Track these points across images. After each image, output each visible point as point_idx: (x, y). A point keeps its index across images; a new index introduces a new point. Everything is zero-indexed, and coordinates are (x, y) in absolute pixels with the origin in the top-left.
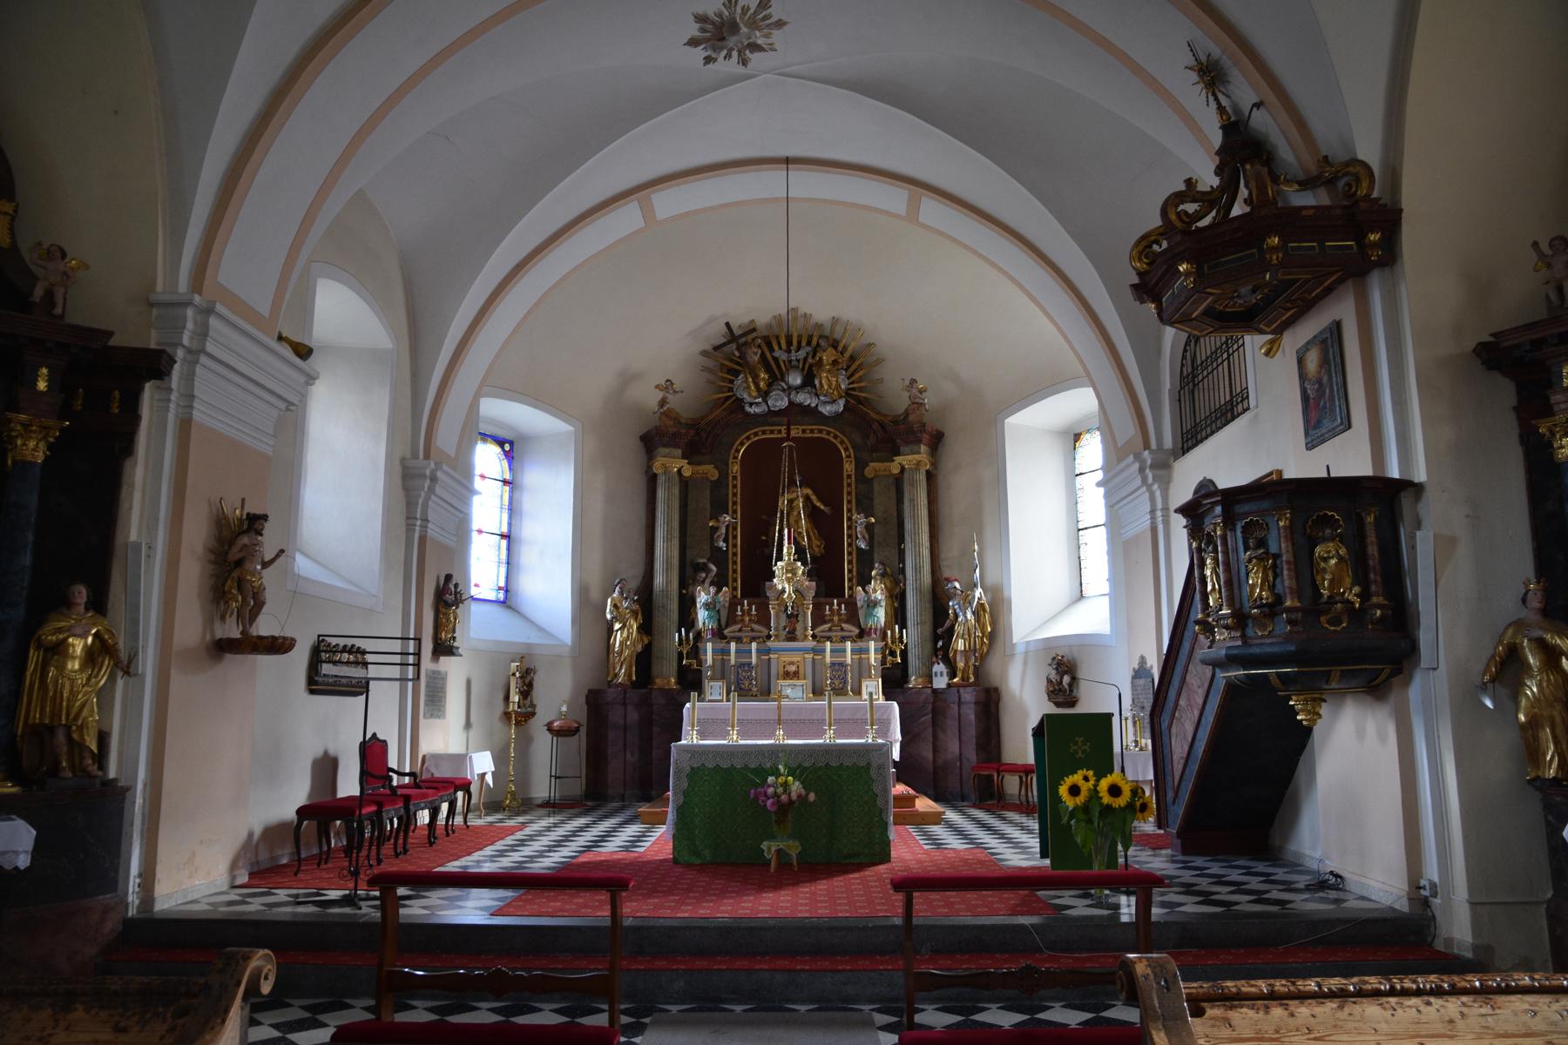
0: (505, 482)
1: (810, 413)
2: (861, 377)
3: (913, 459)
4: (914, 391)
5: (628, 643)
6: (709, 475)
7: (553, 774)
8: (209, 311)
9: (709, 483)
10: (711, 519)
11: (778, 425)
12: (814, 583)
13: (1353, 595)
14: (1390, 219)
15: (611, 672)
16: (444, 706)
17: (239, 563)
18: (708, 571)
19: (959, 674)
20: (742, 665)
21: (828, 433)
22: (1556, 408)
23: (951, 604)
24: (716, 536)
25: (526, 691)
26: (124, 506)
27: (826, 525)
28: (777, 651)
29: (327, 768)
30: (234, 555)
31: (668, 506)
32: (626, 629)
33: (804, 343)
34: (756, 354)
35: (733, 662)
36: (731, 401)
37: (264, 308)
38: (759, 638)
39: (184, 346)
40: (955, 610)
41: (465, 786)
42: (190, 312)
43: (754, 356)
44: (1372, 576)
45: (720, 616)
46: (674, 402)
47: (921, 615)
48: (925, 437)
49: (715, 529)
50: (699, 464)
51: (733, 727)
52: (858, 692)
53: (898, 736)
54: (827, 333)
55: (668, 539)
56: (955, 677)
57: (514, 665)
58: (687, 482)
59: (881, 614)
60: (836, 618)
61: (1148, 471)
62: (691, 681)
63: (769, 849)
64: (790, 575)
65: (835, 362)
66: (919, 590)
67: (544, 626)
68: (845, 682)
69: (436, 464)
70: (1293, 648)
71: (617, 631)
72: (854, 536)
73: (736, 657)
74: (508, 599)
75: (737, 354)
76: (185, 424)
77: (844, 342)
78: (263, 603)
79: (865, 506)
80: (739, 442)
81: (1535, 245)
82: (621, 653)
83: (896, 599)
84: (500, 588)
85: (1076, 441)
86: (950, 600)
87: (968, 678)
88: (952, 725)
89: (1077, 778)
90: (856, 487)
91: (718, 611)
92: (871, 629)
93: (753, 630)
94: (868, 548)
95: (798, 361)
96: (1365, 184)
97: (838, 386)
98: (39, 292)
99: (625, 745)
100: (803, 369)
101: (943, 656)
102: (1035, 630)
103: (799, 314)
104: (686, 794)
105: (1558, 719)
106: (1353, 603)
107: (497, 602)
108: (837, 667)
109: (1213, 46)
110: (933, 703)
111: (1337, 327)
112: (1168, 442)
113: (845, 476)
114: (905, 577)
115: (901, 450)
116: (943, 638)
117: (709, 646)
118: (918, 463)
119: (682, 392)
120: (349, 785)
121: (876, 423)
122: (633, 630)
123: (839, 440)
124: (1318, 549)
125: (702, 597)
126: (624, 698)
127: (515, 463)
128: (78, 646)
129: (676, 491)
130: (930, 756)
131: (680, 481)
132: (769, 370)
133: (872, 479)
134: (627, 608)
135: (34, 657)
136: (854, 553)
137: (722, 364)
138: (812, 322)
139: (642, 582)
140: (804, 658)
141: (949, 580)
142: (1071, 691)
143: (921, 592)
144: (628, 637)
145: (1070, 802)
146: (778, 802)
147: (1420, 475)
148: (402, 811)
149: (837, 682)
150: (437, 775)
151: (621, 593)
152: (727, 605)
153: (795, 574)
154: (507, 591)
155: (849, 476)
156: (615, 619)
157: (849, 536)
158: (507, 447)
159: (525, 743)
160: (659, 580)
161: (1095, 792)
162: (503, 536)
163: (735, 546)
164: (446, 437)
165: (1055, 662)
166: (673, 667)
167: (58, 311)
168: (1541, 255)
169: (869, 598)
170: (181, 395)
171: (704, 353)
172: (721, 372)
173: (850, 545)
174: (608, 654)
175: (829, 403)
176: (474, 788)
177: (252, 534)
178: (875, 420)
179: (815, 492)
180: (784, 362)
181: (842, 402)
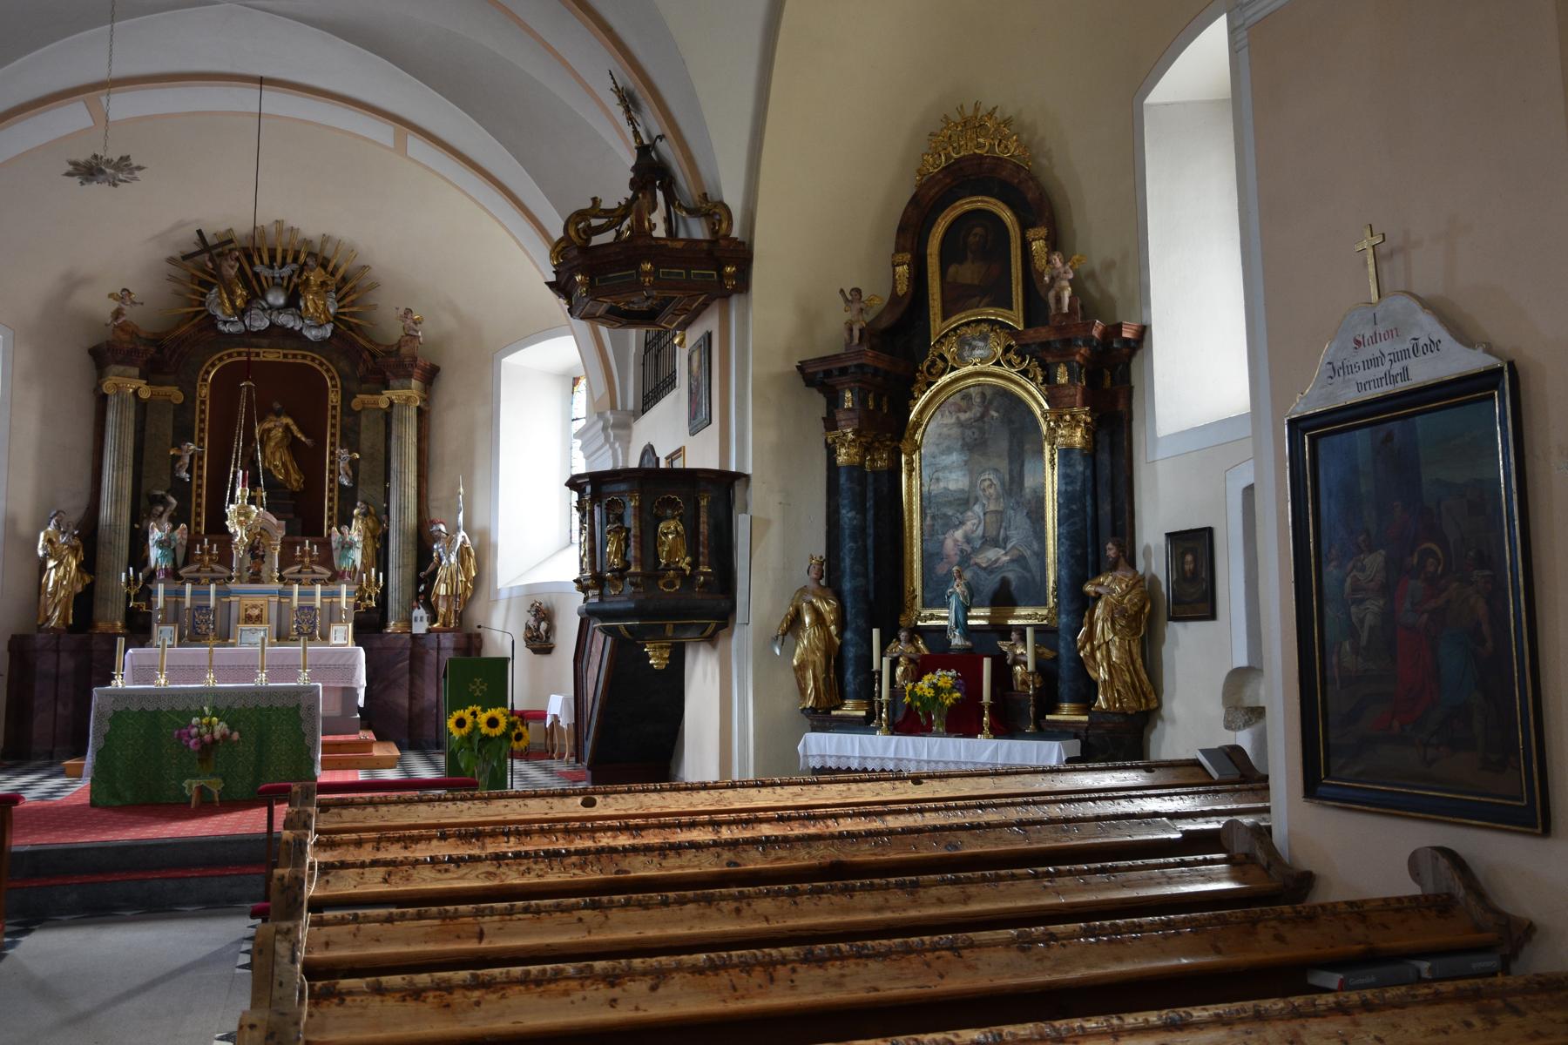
1: (295, 337)
2: (352, 301)
5: (65, 583)
9: (172, 406)
10: (173, 447)
11: (257, 347)
12: (283, 523)
13: (685, 563)
14: (742, 255)
15: (42, 614)
18: (166, 504)
19: (440, 620)
20: (200, 608)
21: (313, 359)
22: (839, 424)
23: (435, 547)
24: (177, 466)
28: (238, 593)
31: (120, 432)
32: (62, 568)
33: (289, 259)
34: (232, 267)
35: (188, 604)
38: (219, 579)
43: (230, 271)
44: (701, 549)
46: (131, 314)
47: (403, 557)
48: (417, 372)
49: (177, 458)
50: (162, 384)
51: (161, 671)
52: (325, 637)
53: (363, 682)
54: (317, 250)
55: (119, 467)
56: (436, 622)
59: (357, 556)
60: (307, 560)
61: (609, 430)
62: (139, 630)
63: (190, 786)
64: (242, 519)
65: (323, 284)
66: (402, 532)
68: (314, 627)
70: (633, 605)
71: (51, 569)
75: (210, 265)
77: (335, 261)
79: (350, 439)
80: (210, 362)
81: (842, 291)
82: (54, 593)
85: (574, 385)
86: (435, 542)
87: (450, 623)
89: (465, 714)
90: (341, 420)
92: (344, 572)
93: (213, 571)
95: (282, 278)
96: (724, 225)
97: (326, 310)
101: (424, 600)
105: (818, 663)
106: (685, 570)
108: (306, 611)
109: (629, 81)
110: (411, 649)
111: (709, 335)
112: (631, 405)
113: (330, 407)
115: (391, 382)
116: (426, 583)
117: (161, 587)
119: (142, 304)
122: (71, 568)
124: (661, 525)
125: (156, 535)
126: (58, 643)
129: (131, 414)
130: (406, 704)
132: (247, 285)
133: (360, 412)
134: (64, 543)
137: (193, 274)
138: (300, 237)
139: (85, 513)
141: (433, 523)
142: (548, 638)
144: (65, 575)
145: (457, 733)
146: (202, 742)
147: (749, 471)
151: (58, 526)
152: (185, 543)
153: (248, 517)
155: (334, 408)
157: (331, 472)
160: (106, 512)
161: (476, 727)
163: (200, 477)
166: (121, 610)
168: (847, 300)
171: (171, 260)
172: (192, 283)
173: (331, 481)
175: (315, 327)
178: (367, 350)
179: (296, 422)
180: (266, 278)
181: (329, 328)
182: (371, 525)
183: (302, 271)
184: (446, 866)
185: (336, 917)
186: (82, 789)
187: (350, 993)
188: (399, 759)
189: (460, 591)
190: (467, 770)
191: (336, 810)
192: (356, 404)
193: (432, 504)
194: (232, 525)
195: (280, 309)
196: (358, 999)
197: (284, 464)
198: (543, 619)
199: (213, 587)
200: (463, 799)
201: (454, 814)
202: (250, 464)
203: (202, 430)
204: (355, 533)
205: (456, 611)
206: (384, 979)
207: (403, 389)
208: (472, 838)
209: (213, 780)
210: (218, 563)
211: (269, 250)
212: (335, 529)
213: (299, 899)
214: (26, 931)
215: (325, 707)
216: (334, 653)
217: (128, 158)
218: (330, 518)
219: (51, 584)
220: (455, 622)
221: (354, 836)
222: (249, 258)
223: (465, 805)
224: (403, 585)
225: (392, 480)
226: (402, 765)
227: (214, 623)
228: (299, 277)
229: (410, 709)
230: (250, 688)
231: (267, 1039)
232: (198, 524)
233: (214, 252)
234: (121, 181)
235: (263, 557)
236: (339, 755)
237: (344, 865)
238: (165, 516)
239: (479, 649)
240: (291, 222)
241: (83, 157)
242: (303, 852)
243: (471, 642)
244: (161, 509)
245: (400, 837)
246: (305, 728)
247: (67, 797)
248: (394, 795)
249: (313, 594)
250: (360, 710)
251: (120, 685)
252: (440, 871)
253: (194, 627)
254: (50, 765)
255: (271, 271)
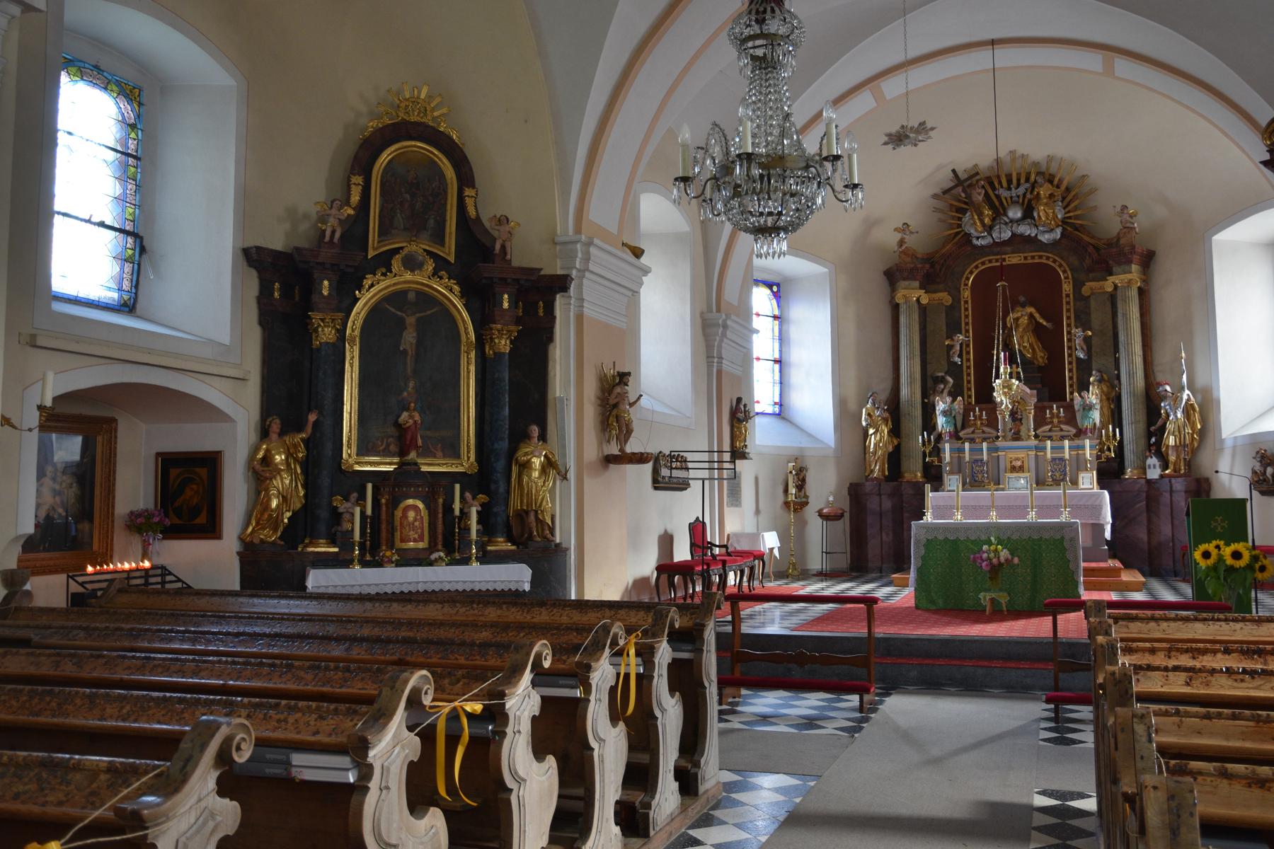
0: (775, 317)
1: (1031, 241)
3: (1127, 278)
4: (1126, 217)
6: (943, 301)
7: (824, 550)
8: (590, 243)
10: (947, 339)
12: (1035, 391)
16: (740, 498)
17: (615, 406)
18: (945, 382)
19: (1171, 466)
20: (976, 461)
21: (1048, 258)
23: (1162, 405)
25: (801, 486)
26: (551, 374)
27: (1050, 338)
28: (1004, 449)
29: (667, 542)
30: (612, 401)
33: (1022, 181)
34: (979, 194)
35: (967, 459)
36: (959, 236)
37: (614, 230)
39: (576, 268)
40: (1166, 411)
41: (760, 556)
42: (579, 246)
45: (955, 421)
46: (911, 241)
47: (1135, 414)
48: (1136, 258)
49: (950, 347)
50: (935, 292)
52: (1075, 483)
53: (1109, 519)
54: (1043, 169)
55: (911, 358)
56: (1167, 469)
57: (791, 465)
58: (925, 308)
59: (1096, 416)
60: (1055, 420)
62: (934, 477)
63: (985, 597)
64: (1006, 390)
65: (1051, 196)
66: (1133, 394)
67: (813, 433)
68: (1065, 475)
69: (726, 315)
72: (1073, 348)
73: (970, 455)
74: (782, 412)
75: (963, 195)
76: (580, 318)
78: (632, 431)
79: (1083, 320)
80: (968, 271)
82: (875, 453)
83: (1113, 401)
84: (776, 403)
86: (1162, 401)
87: (1180, 470)
88: (1165, 510)
89: (1210, 547)
91: (954, 417)
92: (1087, 429)
93: (983, 432)
94: (1086, 357)
95: (1018, 197)
97: (1055, 216)
98: (498, 247)
99: (881, 527)
100: (1023, 204)
101: (1156, 451)
102: (1243, 427)
103: (1017, 155)
104: (923, 558)
107: (774, 414)
108: (1057, 462)
110: (1147, 492)
113: (1064, 295)
114: (1120, 381)
115: (1114, 269)
116: (1156, 435)
117: (947, 446)
118: (1130, 281)
120: (682, 553)
121: (1091, 247)
123: (1057, 264)
125: (941, 406)
126: (879, 489)
127: (782, 303)
128: (537, 462)
129: (916, 317)
130: (1145, 538)
131: (919, 308)
132: (992, 207)
133: (1089, 296)
134: (879, 416)
135: (515, 469)
136: (1074, 365)
137: (951, 205)
138: (1029, 161)
140: (1028, 455)
141: (1159, 384)
143: (1134, 395)
145: (1203, 564)
148: (722, 571)
149: (1057, 475)
150: (739, 548)
151: (874, 404)
152: (961, 411)
153: (1010, 389)
154: (781, 405)
155: (1068, 296)
156: (869, 425)
157: (1069, 348)
158: (775, 289)
159: (802, 524)
160: (904, 392)
161: (1221, 559)
162: (776, 361)
163: (968, 360)
164: (731, 293)
165: (1259, 456)
167: (508, 257)
169: (1085, 402)
170: (576, 299)
171: (935, 196)
173: (1070, 355)
174: (865, 454)
176: (765, 558)
177: (622, 386)
178: (1091, 244)
179: (1038, 310)
180: (1006, 198)
181: (1059, 231)
182: (1105, 389)
183: (1033, 188)
184: (1241, 677)
185: (1160, 709)
186: (907, 595)
187: (1200, 773)
188: (1144, 584)
189: (1187, 442)
190: (1215, 596)
191: (1124, 623)
192: (1085, 291)
193: (1156, 369)
194: (999, 396)
195: (1018, 221)
196: (1209, 779)
197: (1031, 345)
198: (1269, 465)
199: (985, 445)
200: (1235, 620)
201: (1228, 633)
202: (1008, 346)
203: (967, 324)
204: (1093, 396)
205: (1185, 459)
206: (1229, 766)
207: (1125, 273)
208: (1254, 654)
209: (1001, 594)
210: (987, 426)
211: (1006, 175)
212: (1076, 394)
213: (1130, 692)
214: (888, 695)
215: (1083, 539)
216: (1083, 495)
217: (924, 123)
218: (1071, 386)
219: (872, 446)
220: (1185, 469)
221: (1148, 645)
222: (991, 184)
223: (1238, 626)
224: (1136, 439)
225: (1120, 351)
226: (1147, 589)
227: (987, 473)
228: (1031, 193)
229: (1149, 543)
230: (1024, 523)
231: (1168, 799)
232: (970, 397)
233: (966, 184)
234: (920, 141)
235: (1021, 419)
236: (1099, 579)
237: (1150, 668)
238: (946, 391)
239: (1208, 492)
240: (1022, 150)
241: (894, 129)
242: (1115, 655)
243: (1200, 487)
244: (942, 386)
245: (1188, 648)
246: (1069, 556)
247: (898, 601)
248: (1172, 614)
249: (1063, 448)
250: (1107, 542)
251: (930, 520)
252: (1236, 680)
253: (973, 476)
254: (881, 577)
255: (1009, 192)
